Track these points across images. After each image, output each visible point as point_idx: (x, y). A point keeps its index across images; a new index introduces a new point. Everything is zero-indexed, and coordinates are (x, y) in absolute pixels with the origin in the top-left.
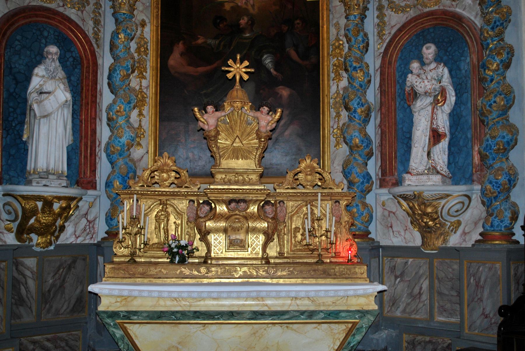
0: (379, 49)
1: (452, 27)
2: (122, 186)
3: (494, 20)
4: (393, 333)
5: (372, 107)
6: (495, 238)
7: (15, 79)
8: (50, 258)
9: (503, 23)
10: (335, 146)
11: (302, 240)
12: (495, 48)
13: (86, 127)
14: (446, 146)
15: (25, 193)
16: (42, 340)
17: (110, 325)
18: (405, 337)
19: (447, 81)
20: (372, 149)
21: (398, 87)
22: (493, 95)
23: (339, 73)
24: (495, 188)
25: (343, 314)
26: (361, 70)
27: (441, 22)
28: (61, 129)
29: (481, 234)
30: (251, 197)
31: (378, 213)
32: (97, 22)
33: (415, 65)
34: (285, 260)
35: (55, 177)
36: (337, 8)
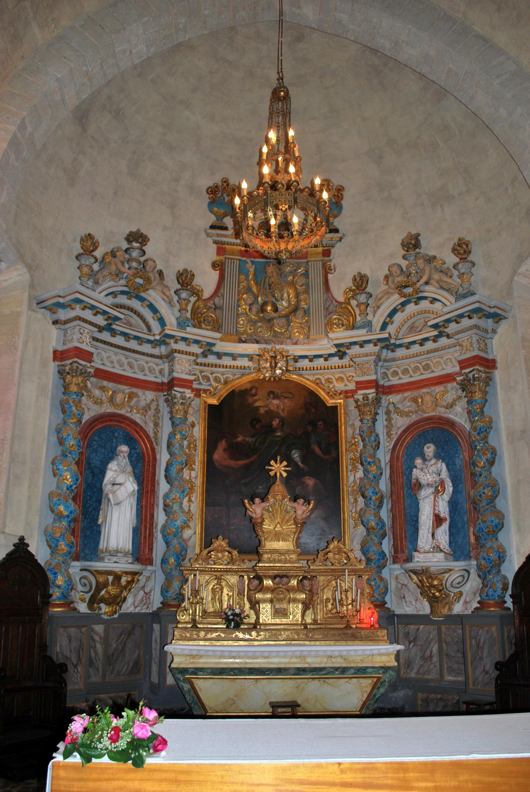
0: (388, 446)
1: (447, 430)
2: (176, 563)
3: (479, 427)
4: (409, 692)
5: (385, 495)
6: (490, 606)
7: (92, 472)
8: (116, 625)
9: (486, 430)
10: (354, 528)
11: (332, 609)
12: (482, 449)
13: (146, 511)
14: (447, 528)
15: (100, 569)
16: (106, 698)
17: (180, 680)
18: (420, 695)
19: (445, 474)
20: (385, 530)
21: (405, 478)
22: (482, 487)
23: (355, 466)
25: (370, 670)
26: (375, 465)
27: (439, 426)
28: (128, 515)
29: (479, 602)
30: (292, 573)
31: (392, 585)
32: (156, 425)
33: (418, 461)
34: (319, 626)
35: (122, 555)
36: (353, 412)
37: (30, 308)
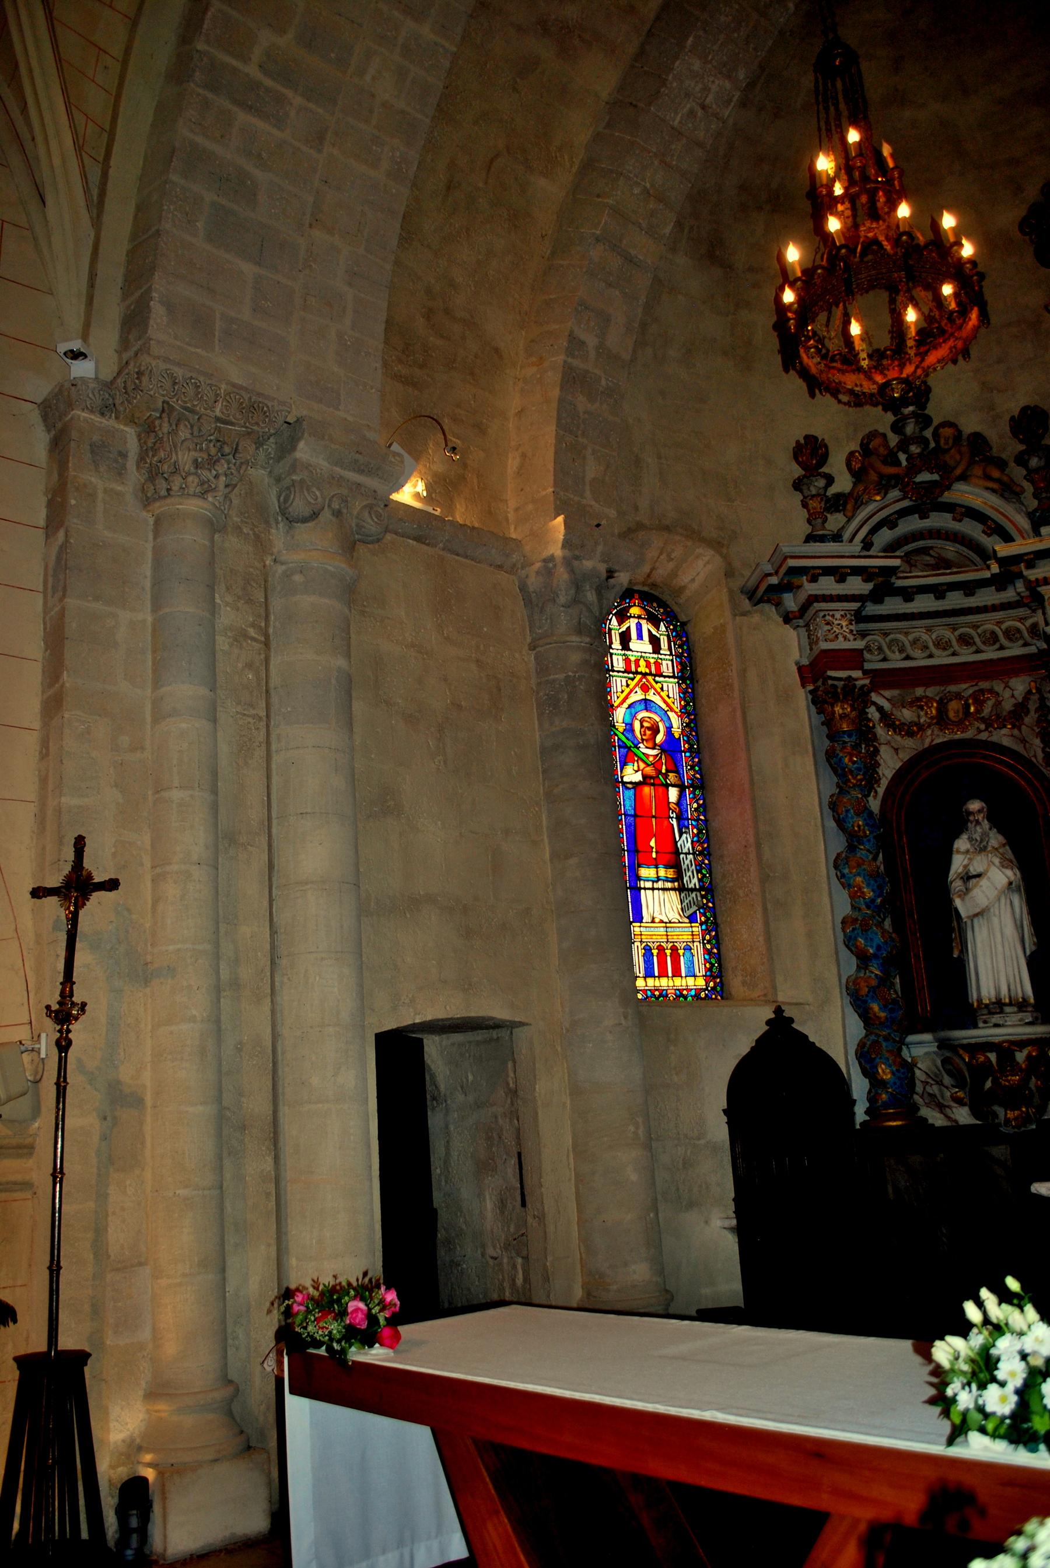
28: (1010, 930)
37: (738, 612)
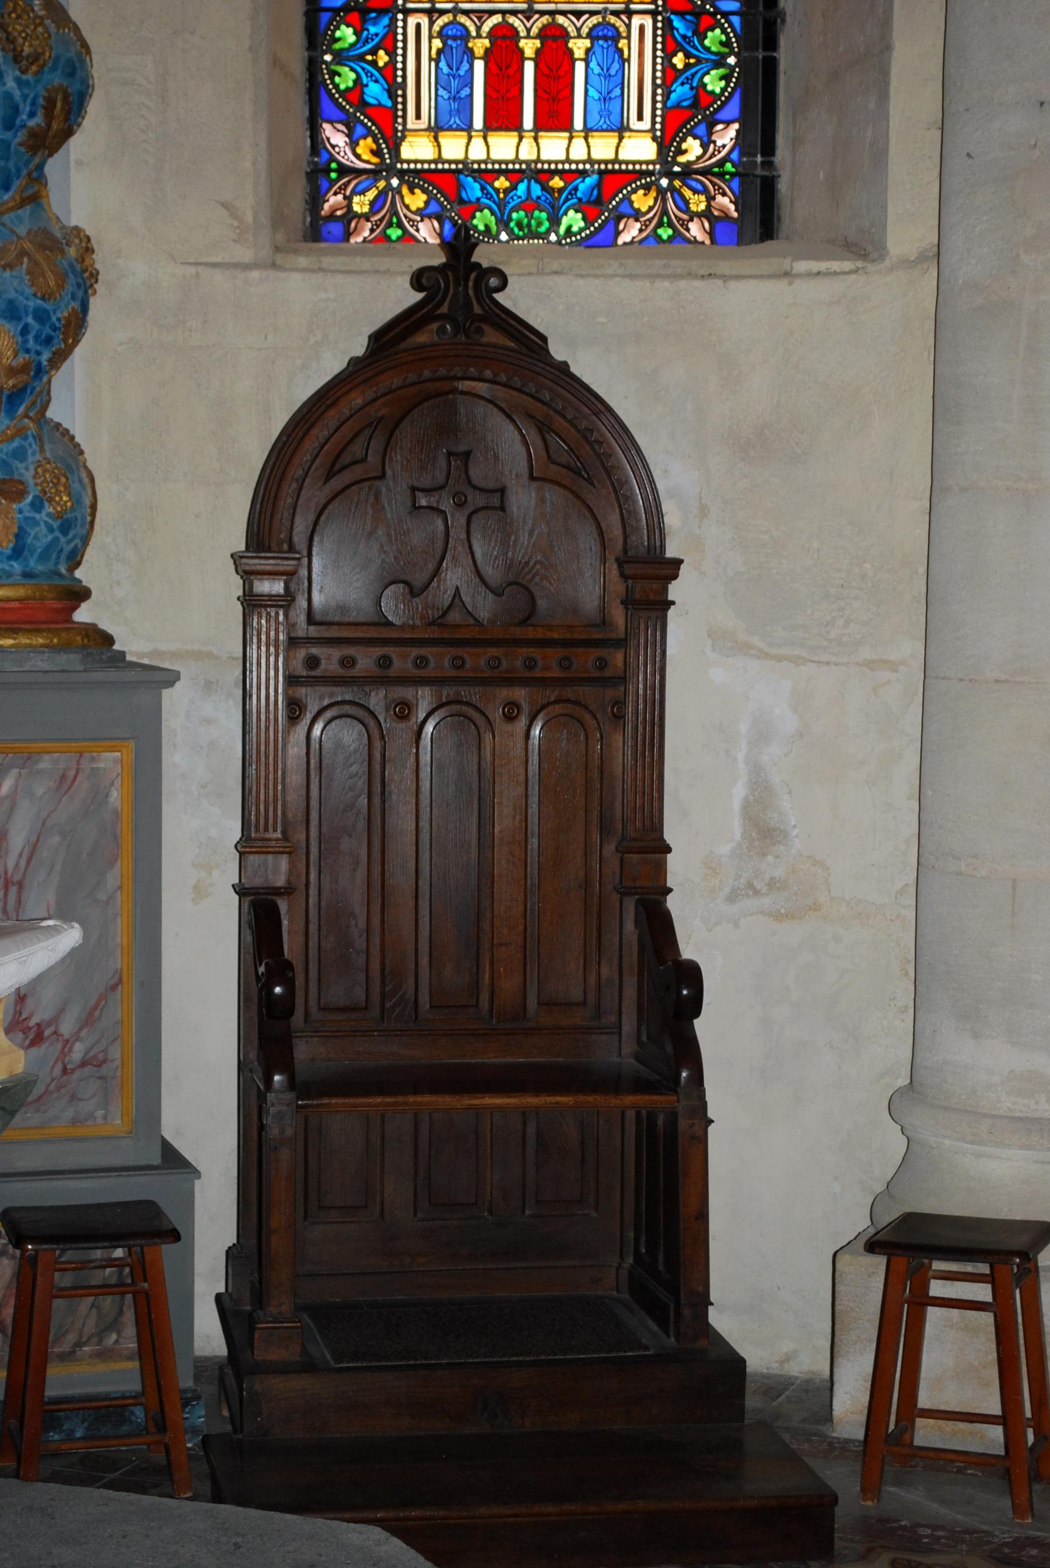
24: (31, 343)
